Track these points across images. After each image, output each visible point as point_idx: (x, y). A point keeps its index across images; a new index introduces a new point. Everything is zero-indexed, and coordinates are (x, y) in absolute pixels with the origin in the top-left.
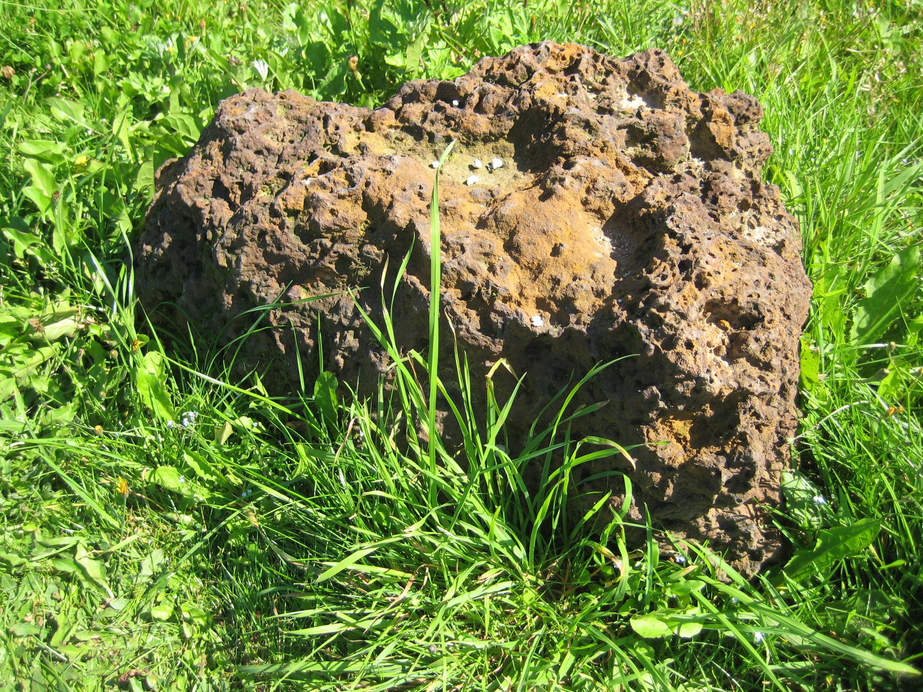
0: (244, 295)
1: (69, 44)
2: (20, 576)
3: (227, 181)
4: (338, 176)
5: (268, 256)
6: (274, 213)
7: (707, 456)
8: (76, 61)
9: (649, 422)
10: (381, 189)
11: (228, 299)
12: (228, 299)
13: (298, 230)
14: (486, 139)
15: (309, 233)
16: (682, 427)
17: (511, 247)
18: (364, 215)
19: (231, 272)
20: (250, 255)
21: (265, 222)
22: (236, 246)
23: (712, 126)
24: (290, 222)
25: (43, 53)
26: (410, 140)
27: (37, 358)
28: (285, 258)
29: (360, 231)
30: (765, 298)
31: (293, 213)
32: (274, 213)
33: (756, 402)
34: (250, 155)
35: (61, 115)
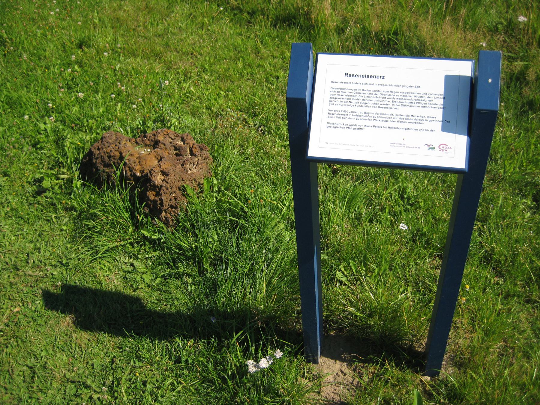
0: (97, 170)
1: (89, 121)
2: (40, 219)
3: (100, 147)
4: (117, 147)
5: (102, 161)
6: (104, 153)
7: (156, 198)
8: (90, 125)
9: (148, 191)
10: (122, 151)
11: (94, 170)
12: (94, 170)
13: (108, 156)
14: (149, 146)
15: (109, 157)
16: (154, 193)
17: (139, 162)
18: (119, 155)
19: (95, 164)
20: (99, 160)
21: (103, 154)
22: (97, 159)
23: (193, 149)
24: (107, 155)
25: (82, 123)
26: (135, 144)
27: (57, 181)
28: (104, 162)
29: (118, 157)
30: (171, 171)
31: (107, 153)
32: (104, 153)
33: (164, 188)
34: (105, 143)
35: (81, 136)
